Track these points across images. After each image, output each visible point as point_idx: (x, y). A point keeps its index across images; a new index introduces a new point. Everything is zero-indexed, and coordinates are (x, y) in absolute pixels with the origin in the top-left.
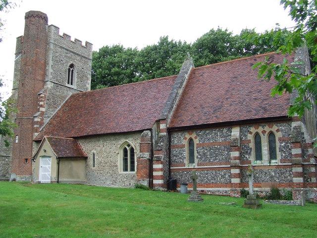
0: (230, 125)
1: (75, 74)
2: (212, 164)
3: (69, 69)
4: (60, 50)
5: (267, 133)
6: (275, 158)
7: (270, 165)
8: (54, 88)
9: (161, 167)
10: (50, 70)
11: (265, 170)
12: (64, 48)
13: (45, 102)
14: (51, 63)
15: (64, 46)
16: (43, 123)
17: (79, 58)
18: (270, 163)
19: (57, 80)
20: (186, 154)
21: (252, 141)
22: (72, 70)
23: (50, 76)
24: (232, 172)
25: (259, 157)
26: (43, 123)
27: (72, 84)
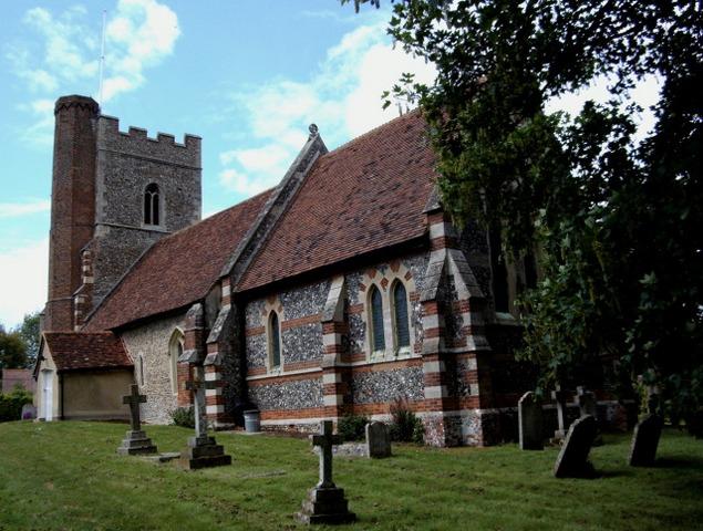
0: (323, 275)
1: (163, 203)
2: (305, 366)
3: (147, 197)
4: (121, 160)
5: (389, 284)
6: (407, 343)
7: (396, 361)
8: (111, 236)
9: (214, 379)
10: (100, 202)
11: (388, 369)
12: (131, 156)
13: (94, 266)
14: (101, 187)
15: (132, 152)
16: (92, 306)
17: (169, 170)
18: (397, 355)
19: (118, 220)
20: (266, 346)
21: (365, 306)
22: (156, 197)
23: (100, 214)
24: (208, 412)
25: (379, 344)
26: (92, 306)
27: (156, 223)
